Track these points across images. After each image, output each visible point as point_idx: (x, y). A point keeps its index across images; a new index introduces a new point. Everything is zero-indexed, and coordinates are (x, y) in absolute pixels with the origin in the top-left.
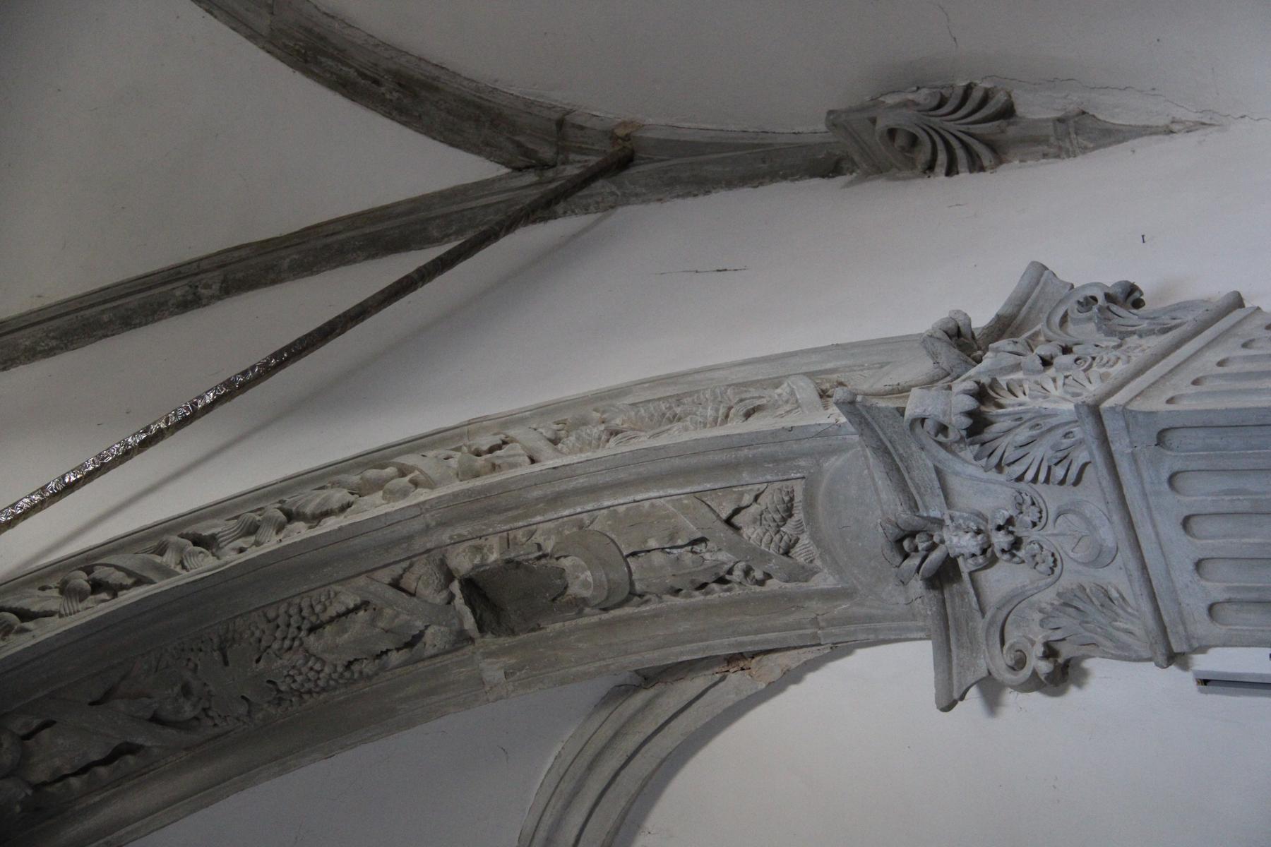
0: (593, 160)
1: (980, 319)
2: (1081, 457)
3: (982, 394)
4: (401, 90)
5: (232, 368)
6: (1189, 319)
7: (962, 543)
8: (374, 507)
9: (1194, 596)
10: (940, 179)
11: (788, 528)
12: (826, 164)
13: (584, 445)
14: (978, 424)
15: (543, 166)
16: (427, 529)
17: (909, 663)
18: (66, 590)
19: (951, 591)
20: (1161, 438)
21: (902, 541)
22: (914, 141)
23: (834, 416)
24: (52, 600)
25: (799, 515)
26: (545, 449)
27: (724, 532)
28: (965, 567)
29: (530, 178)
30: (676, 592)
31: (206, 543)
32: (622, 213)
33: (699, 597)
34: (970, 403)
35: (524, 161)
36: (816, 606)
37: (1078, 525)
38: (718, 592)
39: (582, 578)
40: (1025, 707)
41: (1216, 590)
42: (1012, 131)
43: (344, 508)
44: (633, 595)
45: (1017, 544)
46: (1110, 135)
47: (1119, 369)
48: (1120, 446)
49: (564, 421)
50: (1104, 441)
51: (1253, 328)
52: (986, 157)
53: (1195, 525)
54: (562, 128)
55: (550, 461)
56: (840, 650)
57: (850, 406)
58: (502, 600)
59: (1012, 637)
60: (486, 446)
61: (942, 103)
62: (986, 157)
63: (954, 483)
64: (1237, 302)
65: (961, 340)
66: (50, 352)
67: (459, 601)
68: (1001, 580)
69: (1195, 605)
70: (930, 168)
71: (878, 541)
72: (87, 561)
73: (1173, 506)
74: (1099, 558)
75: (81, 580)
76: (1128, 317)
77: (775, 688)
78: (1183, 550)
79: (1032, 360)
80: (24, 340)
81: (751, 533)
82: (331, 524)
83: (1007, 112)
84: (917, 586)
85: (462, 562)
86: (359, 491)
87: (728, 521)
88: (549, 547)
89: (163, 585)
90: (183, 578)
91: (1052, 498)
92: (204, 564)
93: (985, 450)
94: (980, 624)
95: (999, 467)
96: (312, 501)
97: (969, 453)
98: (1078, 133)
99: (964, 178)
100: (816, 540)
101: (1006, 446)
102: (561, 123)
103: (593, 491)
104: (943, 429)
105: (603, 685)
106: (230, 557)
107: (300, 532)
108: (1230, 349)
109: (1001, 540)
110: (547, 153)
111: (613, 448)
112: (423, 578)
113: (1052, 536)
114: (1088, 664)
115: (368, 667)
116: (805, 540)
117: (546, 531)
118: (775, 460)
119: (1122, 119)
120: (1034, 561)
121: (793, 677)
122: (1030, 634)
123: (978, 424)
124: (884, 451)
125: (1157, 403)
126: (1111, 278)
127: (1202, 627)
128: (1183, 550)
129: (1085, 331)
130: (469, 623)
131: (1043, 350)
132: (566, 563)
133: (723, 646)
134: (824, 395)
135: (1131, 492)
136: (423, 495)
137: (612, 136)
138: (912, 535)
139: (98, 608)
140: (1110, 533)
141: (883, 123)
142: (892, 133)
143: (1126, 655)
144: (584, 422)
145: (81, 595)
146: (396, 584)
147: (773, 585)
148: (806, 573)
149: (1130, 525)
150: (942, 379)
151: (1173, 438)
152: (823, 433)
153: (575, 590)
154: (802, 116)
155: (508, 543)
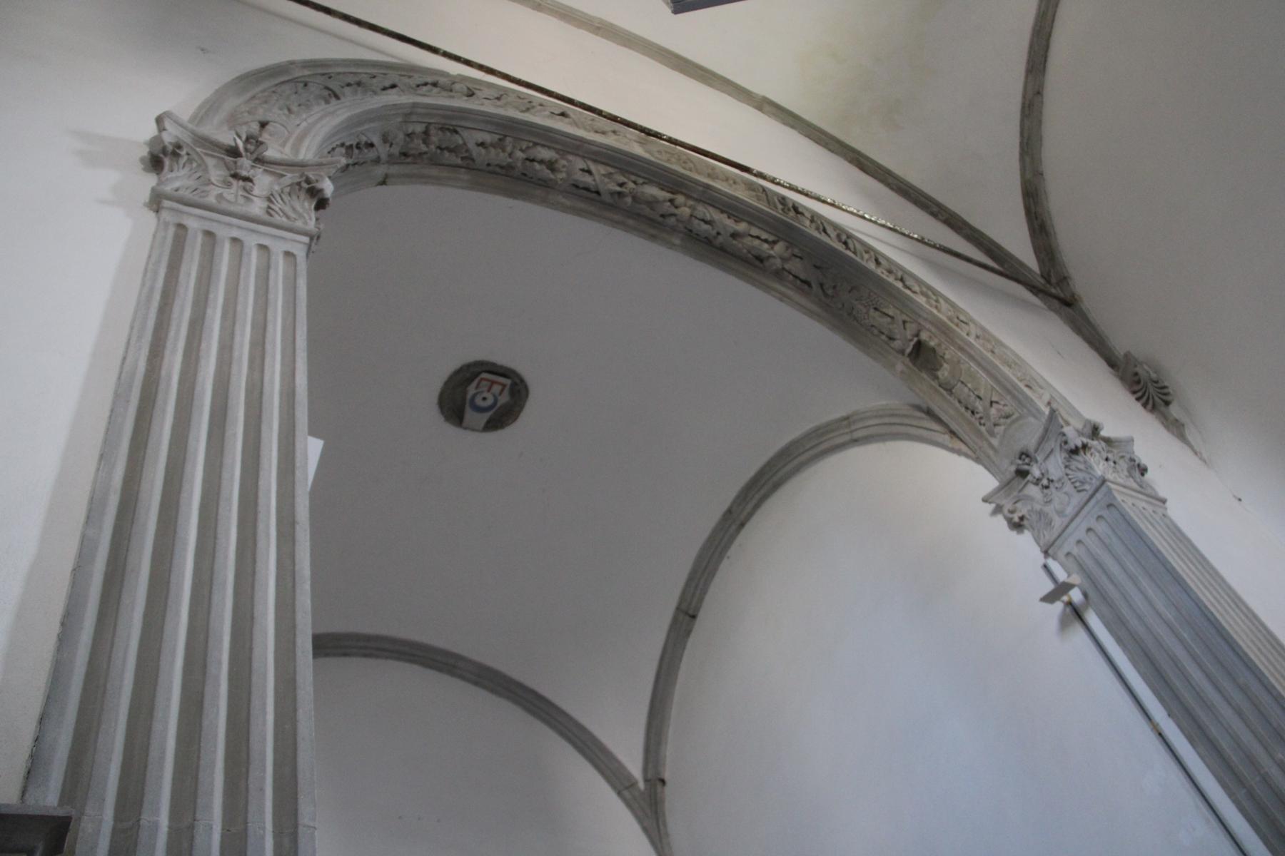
0: (1062, 295)
1: (1104, 433)
2: (1087, 487)
3: (1085, 446)
4: (1039, 227)
5: (927, 237)
6: (1149, 491)
7: (1036, 471)
8: (921, 300)
9: (1069, 545)
10: (1132, 398)
11: (1002, 420)
12: (1112, 362)
13: (983, 345)
14: (1075, 451)
15: (1049, 282)
16: (926, 320)
17: (989, 482)
18: (838, 236)
19: (1018, 479)
20: (1109, 506)
21: (1024, 454)
22: (1138, 382)
23: (1047, 411)
24: (833, 235)
25: (1008, 421)
26: (973, 336)
27: (988, 404)
28: (1029, 477)
29: (1042, 281)
30: (960, 402)
31: (878, 263)
32: (1052, 314)
33: (963, 410)
34: (1080, 444)
35: (1046, 276)
36: (985, 445)
37: (1065, 500)
38: (968, 414)
39: (944, 373)
40: (1000, 521)
41: (1075, 551)
42: (1163, 408)
43: (914, 292)
44: (950, 391)
45: (1047, 487)
46: (1182, 437)
47: (1120, 481)
48: (1098, 496)
49: (984, 335)
50: (1096, 490)
51: (1160, 511)
52: (1150, 406)
53: (1091, 534)
54: (1064, 280)
55: (971, 339)
56: (978, 460)
57: (1053, 412)
58: (922, 356)
59: (1018, 505)
60: (962, 320)
61: (1156, 382)
62: (1150, 406)
63: (1052, 458)
64: (1164, 501)
65: (1095, 431)
66: (892, 189)
67: (912, 344)
68: (1033, 491)
69: (1066, 549)
70: (1134, 392)
71: (1018, 448)
72: (849, 236)
73: (1092, 523)
74: (1060, 513)
75: (844, 237)
76: (1137, 474)
77: (952, 450)
78: (1080, 534)
79: (1105, 455)
80: (890, 180)
81: (993, 411)
82: (908, 292)
83: (1167, 403)
84: (1013, 468)
85: (924, 336)
86: (923, 294)
87: (992, 402)
88: (947, 357)
89: (858, 259)
90: (864, 263)
91: (1068, 487)
92: (871, 266)
93: (1069, 459)
94: (1015, 493)
95: (1066, 467)
96: (910, 282)
97: (1064, 455)
98: (1176, 428)
99: (1138, 406)
100: (1005, 431)
101: (1074, 464)
102: (1065, 278)
103: (972, 357)
104: (1066, 443)
105: (917, 401)
106: (879, 271)
107: (899, 285)
108: (1150, 509)
109: (1045, 482)
110: (1053, 280)
111: (989, 355)
112: (911, 329)
113: (1057, 497)
114: (1026, 532)
115: (876, 332)
116: (1002, 428)
117: (950, 353)
118: (1020, 402)
119: (1190, 438)
120: (1046, 495)
121: (959, 452)
122: (1023, 509)
123: (1075, 451)
124: (1046, 430)
125: (1119, 498)
126: (1144, 461)
127: (1061, 555)
128: (1080, 534)
129: (1123, 465)
130: (908, 350)
131: (1110, 456)
132: (945, 365)
133: (954, 427)
134: (1049, 403)
135: (1086, 509)
136: (935, 311)
137: (1073, 295)
138: (1028, 456)
139: (840, 247)
140: (1070, 511)
141: (1138, 369)
142: (1136, 374)
143: (1037, 541)
144: (989, 341)
145: (840, 241)
146: (904, 322)
147: (983, 429)
148: (992, 434)
149: (1077, 515)
150: (1080, 433)
151: (1112, 509)
152: (1038, 410)
153: (939, 374)
154: (1121, 345)
155: (939, 345)
